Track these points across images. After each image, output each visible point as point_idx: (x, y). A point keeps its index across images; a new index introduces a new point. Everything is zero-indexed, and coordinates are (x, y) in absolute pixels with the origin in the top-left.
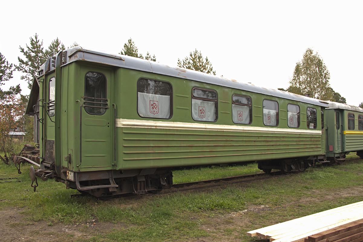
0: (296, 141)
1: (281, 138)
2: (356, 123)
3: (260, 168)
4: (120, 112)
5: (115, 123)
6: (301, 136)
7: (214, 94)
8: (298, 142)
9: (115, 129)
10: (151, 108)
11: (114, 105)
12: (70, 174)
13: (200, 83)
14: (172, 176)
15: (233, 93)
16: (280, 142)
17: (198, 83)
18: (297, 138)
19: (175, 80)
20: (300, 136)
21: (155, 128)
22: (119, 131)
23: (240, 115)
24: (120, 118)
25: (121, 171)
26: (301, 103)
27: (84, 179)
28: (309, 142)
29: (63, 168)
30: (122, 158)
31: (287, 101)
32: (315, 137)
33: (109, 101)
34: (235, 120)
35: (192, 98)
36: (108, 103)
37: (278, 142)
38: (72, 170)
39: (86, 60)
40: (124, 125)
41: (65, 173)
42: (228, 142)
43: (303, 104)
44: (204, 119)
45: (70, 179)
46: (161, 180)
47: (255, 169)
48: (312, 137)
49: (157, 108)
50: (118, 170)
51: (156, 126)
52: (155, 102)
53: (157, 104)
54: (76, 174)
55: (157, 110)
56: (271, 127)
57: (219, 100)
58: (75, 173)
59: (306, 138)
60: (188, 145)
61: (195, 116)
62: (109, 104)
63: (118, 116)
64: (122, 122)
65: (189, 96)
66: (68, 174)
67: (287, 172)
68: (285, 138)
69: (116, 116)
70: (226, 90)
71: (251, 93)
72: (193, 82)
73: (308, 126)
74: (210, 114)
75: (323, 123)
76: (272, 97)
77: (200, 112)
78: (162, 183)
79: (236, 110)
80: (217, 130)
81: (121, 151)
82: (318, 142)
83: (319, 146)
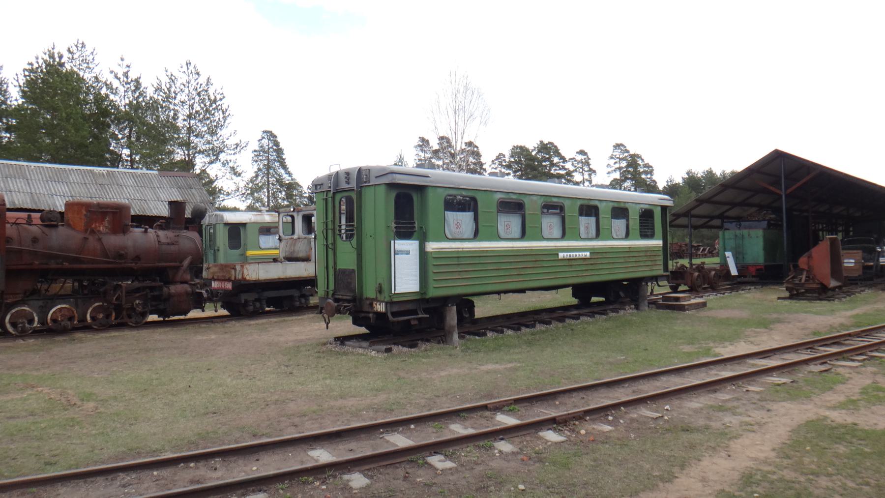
1: (604, 254)
2: (584, 212)
3: (575, 295)
4: (430, 234)
7: (562, 208)
8: (627, 259)
11: (421, 227)
12: (380, 305)
14: (474, 306)
19: (480, 193)
20: (630, 250)
21: (461, 250)
23: (508, 227)
24: (429, 242)
25: (427, 301)
26: (631, 204)
27: (395, 309)
29: (368, 299)
30: (432, 284)
33: (416, 223)
34: (502, 233)
35: (498, 212)
36: (416, 225)
37: (599, 260)
38: (382, 300)
40: (433, 249)
41: (371, 304)
42: (537, 263)
43: (634, 205)
47: (566, 297)
48: (647, 250)
51: (463, 248)
54: (389, 305)
56: (469, 242)
57: (527, 212)
58: (386, 303)
70: (535, 198)
74: (557, 232)
81: (431, 277)
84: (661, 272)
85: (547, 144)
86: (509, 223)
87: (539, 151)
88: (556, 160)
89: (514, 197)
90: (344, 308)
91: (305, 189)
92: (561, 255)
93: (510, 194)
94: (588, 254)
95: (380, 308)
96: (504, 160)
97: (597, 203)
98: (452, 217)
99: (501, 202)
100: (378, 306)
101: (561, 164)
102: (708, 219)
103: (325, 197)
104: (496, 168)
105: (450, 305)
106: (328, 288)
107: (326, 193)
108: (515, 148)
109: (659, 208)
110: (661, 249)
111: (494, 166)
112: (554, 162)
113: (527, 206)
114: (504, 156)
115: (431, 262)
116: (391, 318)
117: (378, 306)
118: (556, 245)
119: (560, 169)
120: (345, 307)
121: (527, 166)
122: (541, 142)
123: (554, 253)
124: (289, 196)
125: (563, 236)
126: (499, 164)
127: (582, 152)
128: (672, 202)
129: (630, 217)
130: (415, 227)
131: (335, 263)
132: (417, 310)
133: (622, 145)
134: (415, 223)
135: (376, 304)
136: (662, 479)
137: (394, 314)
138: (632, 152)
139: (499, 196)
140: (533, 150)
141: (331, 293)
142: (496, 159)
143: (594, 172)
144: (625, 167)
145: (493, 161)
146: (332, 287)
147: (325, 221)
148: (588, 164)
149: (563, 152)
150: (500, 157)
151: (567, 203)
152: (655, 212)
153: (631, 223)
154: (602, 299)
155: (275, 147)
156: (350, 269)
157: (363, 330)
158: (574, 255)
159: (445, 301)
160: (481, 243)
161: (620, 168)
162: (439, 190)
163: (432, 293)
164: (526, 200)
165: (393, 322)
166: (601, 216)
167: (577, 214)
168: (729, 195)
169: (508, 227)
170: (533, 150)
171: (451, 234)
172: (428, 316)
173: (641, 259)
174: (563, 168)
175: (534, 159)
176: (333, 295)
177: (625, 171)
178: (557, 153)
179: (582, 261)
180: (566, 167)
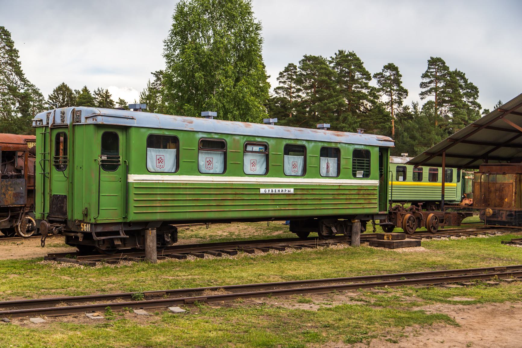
0: (333, 194)
1: (310, 191)
3: (292, 230)
4: (132, 168)
5: (127, 178)
6: (341, 188)
7: (266, 147)
9: (127, 185)
10: (157, 162)
11: (125, 162)
12: (86, 226)
13: (208, 134)
15: (245, 140)
16: (307, 195)
17: (206, 134)
18: (335, 190)
20: (339, 188)
21: (162, 182)
22: (131, 185)
24: (131, 174)
25: (130, 224)
26: (344, 145)
27: (99, 229)
28: (356, 195)
31: (320, 144)
32: (365, 190)
33: (121, 158)
35: (199, 150)
36: (121, 159)
38: (88, 222)
39: (105, 123)
40: (135, 180)
42: (237, 196)
43: (347, 145)
44: (211, 171)
45: (85, 230)
46: (165, 236)
48: (360, 190)
49: (163, 163)
50: (129, 222)
52: (161, 157)
53: (163, 159)
55: (163, 164)
57: (228, 150)
58: (92, 224)
59: (350, 191)
60: (194, 199)
61: (203, 169)
62: (121, 161)
63: (130, 172)
64: (133, 178)
65: (241, 150)
66: (82, 226)
67: (326, 236)
68: (314, 190)
69: (127, 171)
70: (237, 138)
71: (268, 138)
72: (200, 133)
73: (354, 175)
75: (58, 158)
76: (296, 141)
77: (157, 161)
78: (166, 239)
79: (203, 159)
80: (225, 183)
82: (372, 195)
83: (373, 201)
84: (377, 211)
85: (347, 56)
86: (211, 159)
87: (338, 64)
88: (358, 75)
89: (216, 136)
90: (56, 228)
91: (46, 98)
92: (262, 191)
93: (213, 134)
94: (292, 190)
95: (86, 228)
96: (295, 72)
97: (304, 143)
98: (153, 154)
99: (202, 141)
100: (85, 227)
101: (364, 81)
102: (472, 159)
103: (43, 132)
104: (284, 82)
105: (150, 229)
106: (44, 212)
107: (44, 128)
108: (307, 58)
109: (378, 149)
110: (378, 188)
111: (282, 80)
112: (356, 77)
113: (228, 145)
114: (295, 67)
115: (132, 191)
116: (95, 238)
117: (85, 227)
118: (258, 181)
119: (362, 88)
120: (57, 227)
121: (321, 83)
122: (341, 52)
123: (256, 188)
124: (24, 109)
125: (267, 173)
126: (288, 78)
127: (391, 67)
128: (393, 143)
129: (342, 157)
130: (119, 161)
131: (51, 190)
132: (119, 231)
133: (439, 60)
134: (119, 157)
135: (83, 225)
136: (204, 314)
137: (99, 234)
138: (452, 69)
139: (201, 135)
140: (331, 62)
141: (46, 215)
142: (285, 72)
143: (406, 92)
144: (442, 87)
145: (281, 73)
146: (47, 210)
147: (43, 152)
148: (397, 82)
149: (367, 66)
150: (290, 68)
151: (271, 143)
152: (371, 152)
153: (343, 162)
154: (343, 235)
155: (7, 48)
156: (63, 195)
157: (74, 249)
158: (276, 190)
159: (146, 225)
160: (181, 176)
161: (436, 89)
162: (143, 130)
163: (132, 217)
164: (228, 140)
165: (99, 241)
166: (308, 155)
167: (282, 152)
168: (483, 135)
169: (209, 163)
170: (331, 62)
171: (153, 167)
172: (128, 237)
173: (352, 197)
174: (366, 86)
175: (329, 74)
176: (48, 217)
177: (443, 92)
178: (359, 66)
179: (270, 195)
180: (370, 85)
